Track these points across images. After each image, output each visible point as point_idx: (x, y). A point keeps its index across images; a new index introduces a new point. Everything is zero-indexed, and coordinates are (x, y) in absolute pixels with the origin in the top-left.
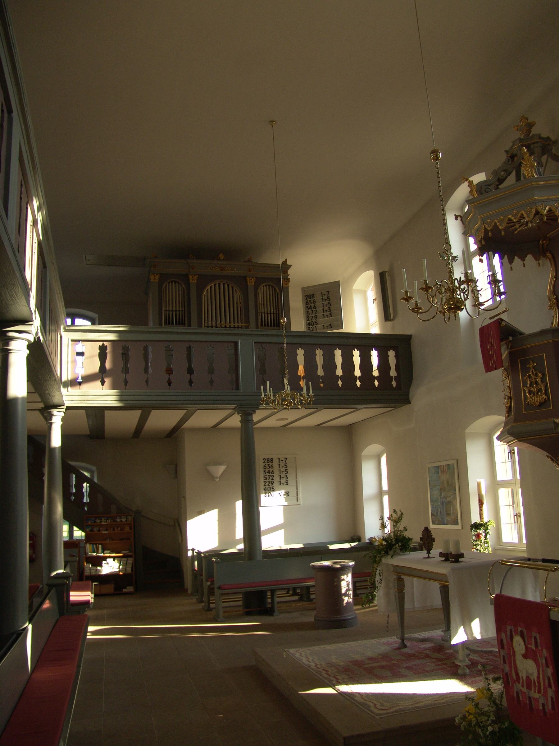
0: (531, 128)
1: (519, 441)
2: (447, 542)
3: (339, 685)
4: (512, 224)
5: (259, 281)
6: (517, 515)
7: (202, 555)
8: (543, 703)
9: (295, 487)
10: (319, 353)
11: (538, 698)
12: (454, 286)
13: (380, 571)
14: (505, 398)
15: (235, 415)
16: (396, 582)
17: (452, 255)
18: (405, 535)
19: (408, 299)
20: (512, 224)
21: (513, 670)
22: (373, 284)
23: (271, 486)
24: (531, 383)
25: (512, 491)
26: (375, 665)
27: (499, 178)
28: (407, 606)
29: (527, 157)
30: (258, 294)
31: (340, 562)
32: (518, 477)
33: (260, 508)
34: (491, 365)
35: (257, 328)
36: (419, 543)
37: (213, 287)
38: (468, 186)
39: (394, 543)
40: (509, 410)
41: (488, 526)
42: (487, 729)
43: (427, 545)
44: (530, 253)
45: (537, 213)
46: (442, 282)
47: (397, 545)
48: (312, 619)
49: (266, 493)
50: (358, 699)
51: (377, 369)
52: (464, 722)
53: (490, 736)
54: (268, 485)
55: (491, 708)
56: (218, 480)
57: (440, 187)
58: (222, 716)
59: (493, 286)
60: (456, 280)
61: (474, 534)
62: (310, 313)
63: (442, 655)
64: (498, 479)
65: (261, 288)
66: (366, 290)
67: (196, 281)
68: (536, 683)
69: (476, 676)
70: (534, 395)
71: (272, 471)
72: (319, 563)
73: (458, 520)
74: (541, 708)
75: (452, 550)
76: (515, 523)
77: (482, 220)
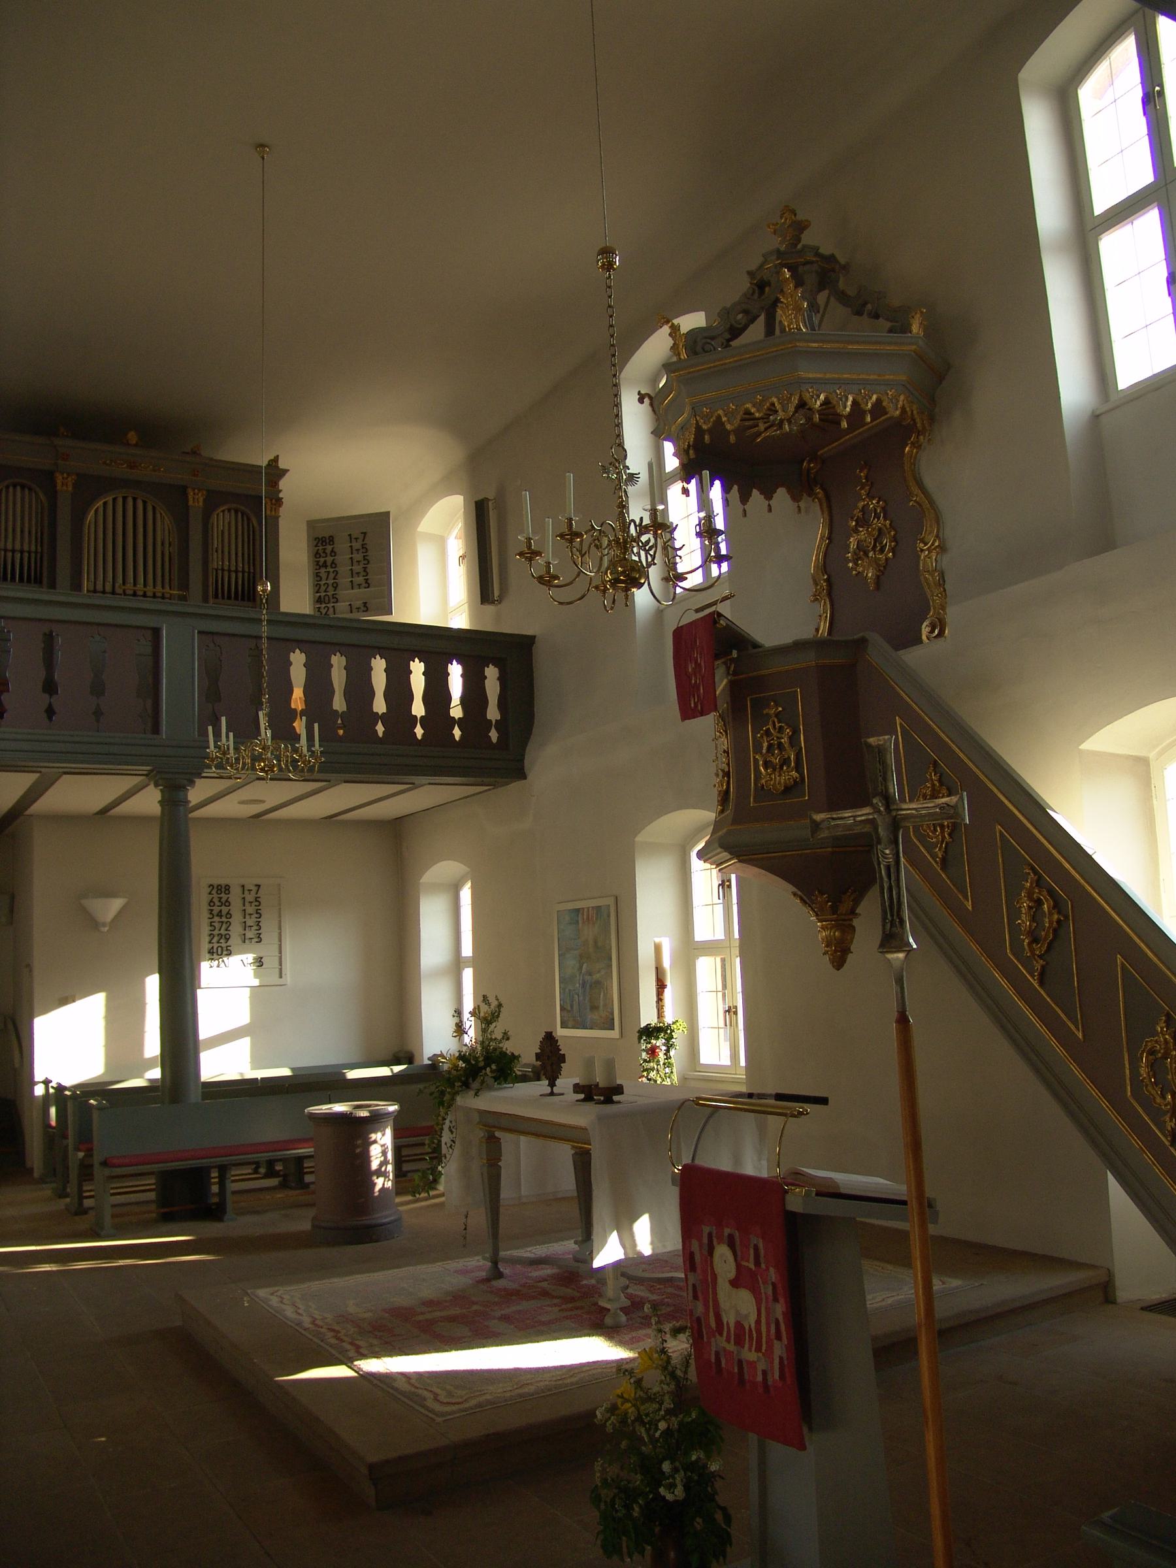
0: (803, 233)
1: (740, 861)
2: (589, 1064)
3: (360, 1360)
4: (751, 423)
5: (214, 499)
6: (731, 1011)
7: (67, 1093)
8: (764, 1368)
9: (276, 946)
10: (338, 662)
11: (756, 1360)
12: (628, 536)
13: (451, 1122)
14: (717, 775)
15: (149, 787)
16: (484, 1145)
17: (628, 471)
18: (504, 1049)
19: (531, 554)
20: (751, 423)
21: (711, 1310)
22: (460, 525)
23: (224, 945)
24: (770, 746)
25: (723, 960)
26: (438, 1314)
27: (731, 325)
28: (506, 1193)
29: (789, 289)
30: (210, 527)
31: (369, 1106)
32: (737, 936)
33: (199, 992)
34: (693, 705)
35: (205, 599)
36: (534, 1067)
37: (111, 503)
38: (670, 335)
39: (482, 1064)
40: (724, 798)
41: (672, 1031)
42: (657, 1425)
43: (549, 1068)
44: (782, 486)
45: (802, 405)
46: (604, 526)
47: (488, 1069)
48: (306, 1226)
49: (212, 959)
50: (402, 1385)
51: (459, 703)
52: (612, 1417)
53: (661, 1440)
54: (218, 942)
55: (665, 1387)
56: (106, 929)
57: (611, 326)
58: (103, 1439)
59: (707, 542)
60: (632, 523)
61: (644, 1047)
62: (324, 576)
63: (574, 1289)
64: (697, 938)
65: (218, 515)
66: (446, 535)
67: (70, 489)
68: (754, 1332)
69: (640, 1328)
70: (774, 770)
71: (228, 913)
72: (324, 1108)
73: (613, 1019)
74: (760, 1378)
75: (600, 1079)
76: (726, 1025)
77: (692, 409)
